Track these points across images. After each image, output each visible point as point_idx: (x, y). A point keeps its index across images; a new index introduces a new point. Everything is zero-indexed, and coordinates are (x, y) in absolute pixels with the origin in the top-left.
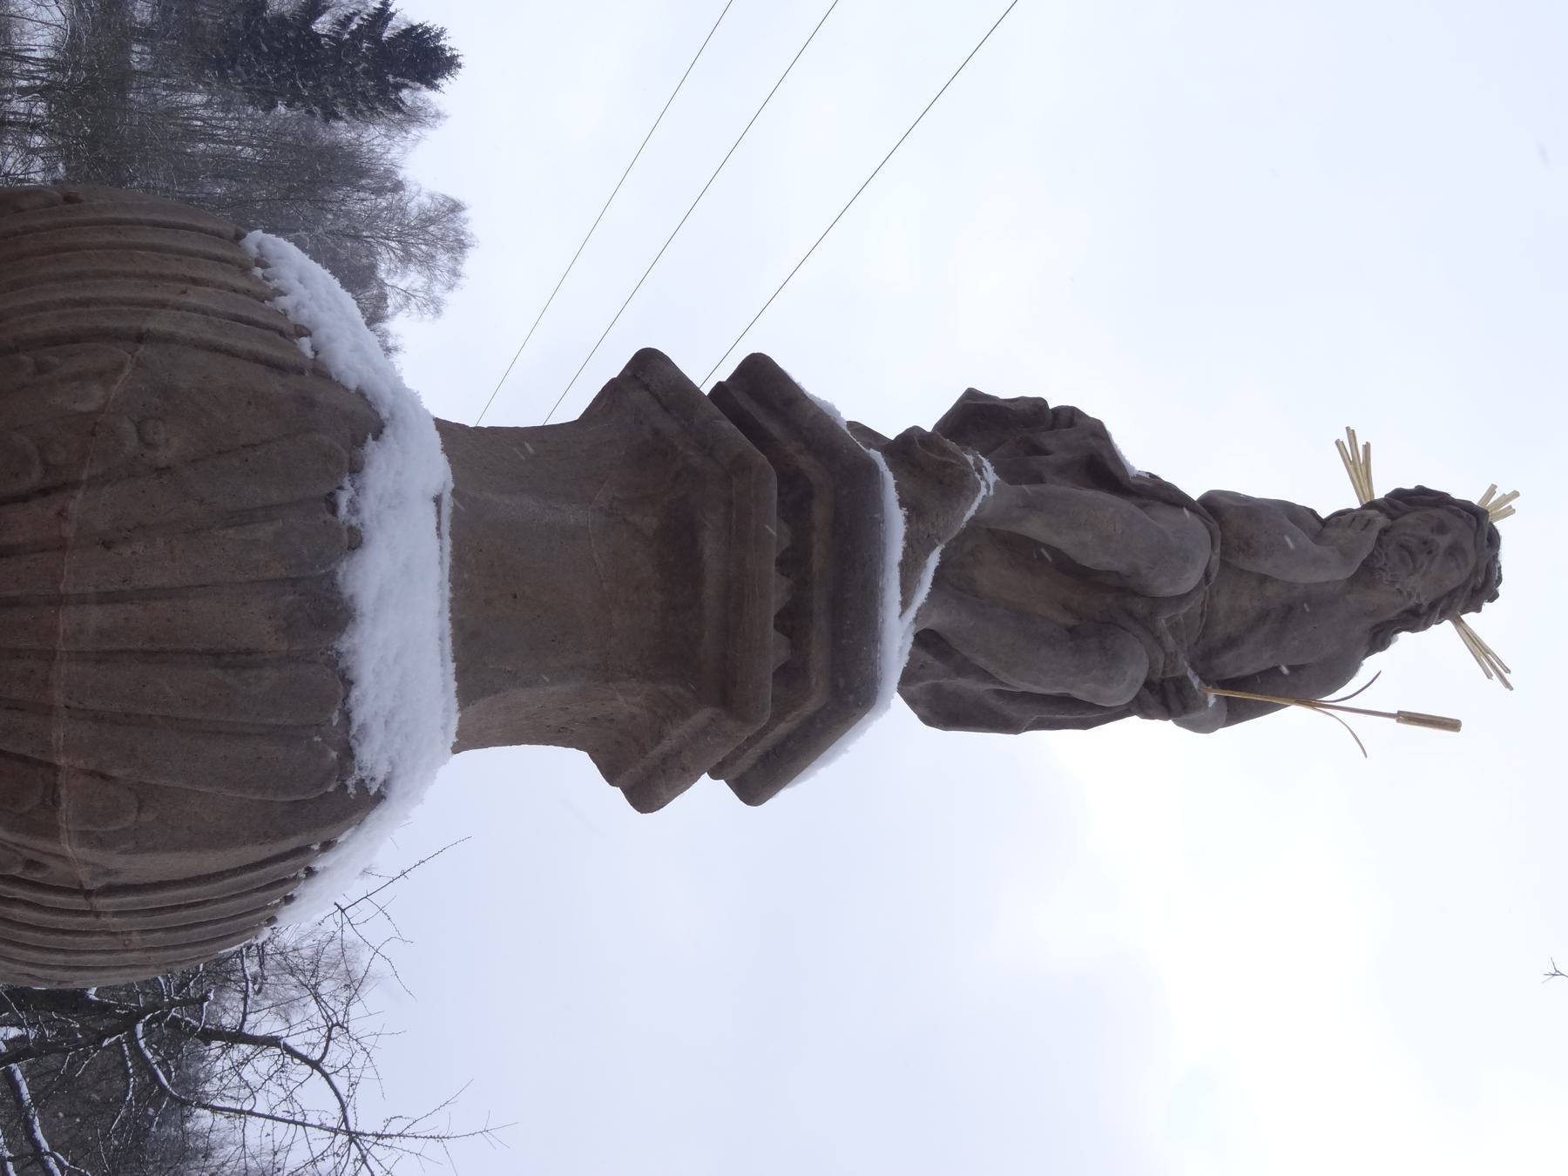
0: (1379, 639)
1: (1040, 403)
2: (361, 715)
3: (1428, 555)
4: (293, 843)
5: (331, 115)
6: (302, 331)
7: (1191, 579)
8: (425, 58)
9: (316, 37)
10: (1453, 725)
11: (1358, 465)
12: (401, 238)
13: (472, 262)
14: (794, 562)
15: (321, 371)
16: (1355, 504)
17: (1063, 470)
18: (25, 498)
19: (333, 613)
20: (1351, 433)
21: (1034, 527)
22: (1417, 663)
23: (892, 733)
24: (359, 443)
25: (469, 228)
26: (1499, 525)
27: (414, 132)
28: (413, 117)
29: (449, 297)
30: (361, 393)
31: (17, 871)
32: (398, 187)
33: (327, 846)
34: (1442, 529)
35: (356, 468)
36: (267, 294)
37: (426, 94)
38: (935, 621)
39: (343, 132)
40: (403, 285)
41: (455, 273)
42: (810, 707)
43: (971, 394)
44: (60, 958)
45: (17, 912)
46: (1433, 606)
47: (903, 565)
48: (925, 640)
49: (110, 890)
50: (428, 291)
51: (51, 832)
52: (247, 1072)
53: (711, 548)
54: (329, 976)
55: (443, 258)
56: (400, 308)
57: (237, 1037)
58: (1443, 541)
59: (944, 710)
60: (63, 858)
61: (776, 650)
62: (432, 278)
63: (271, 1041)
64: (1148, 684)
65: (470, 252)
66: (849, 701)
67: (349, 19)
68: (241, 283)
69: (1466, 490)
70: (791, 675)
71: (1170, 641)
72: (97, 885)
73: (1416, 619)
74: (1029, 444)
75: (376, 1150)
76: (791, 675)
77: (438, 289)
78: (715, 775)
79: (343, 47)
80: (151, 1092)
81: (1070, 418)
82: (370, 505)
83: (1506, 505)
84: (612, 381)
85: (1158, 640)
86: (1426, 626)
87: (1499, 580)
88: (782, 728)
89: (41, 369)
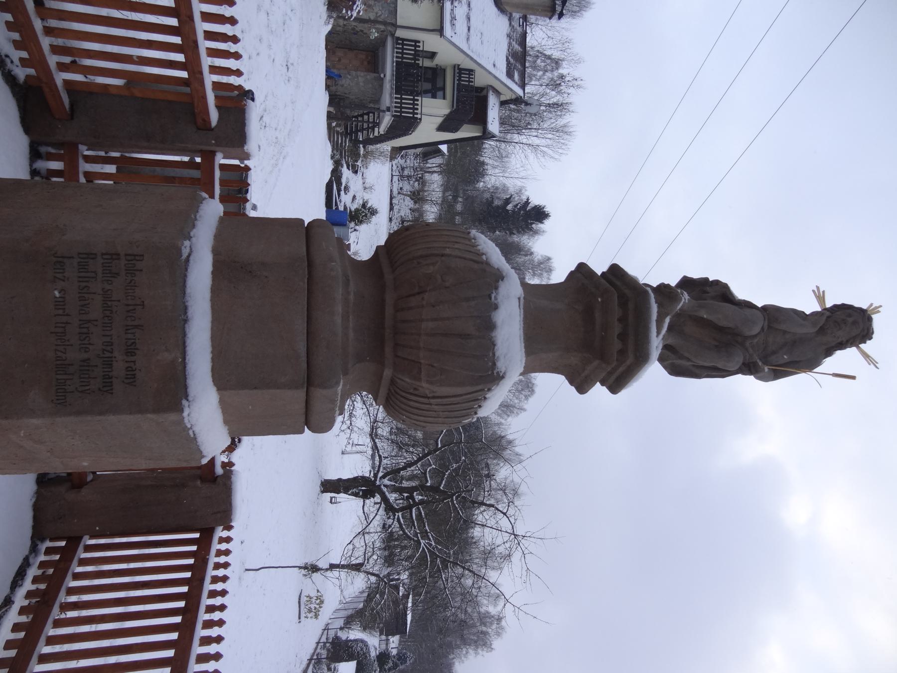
0: (829, 353)
1: (707, 279)
2: (497, 354)
3: (846, 326)
4: (480, 387)
5: (512, 233)
6: (483, 254)
7: (756, 330)
8: (540, 214)
9: (508, 211)
10: (853, 378)
11: (821, 298)
12: (532, 269)
14: (623, 320)
15: (488, 263)
16: (819, 309)
17: (713, 298)
18: (414, 295)
19: (489, 326)
20: (818, 288)
22: (844, 359)
23: (654, 372)
24: (498, 281)
25: (553, 265)
26: (873, 316)
27: (536, 237)
28: (536, 232)
30: (498, 269)
31: (411, 391)
32: (532, 254)
33: (489, 390)
34: (850, 316)
35: (496, 288)
36: (475, 246)
37: (540, 225)
38: (670, 341)
39: (515, 238)
42: (628, 362)
43: (685, 277)
44: (422, 418)
45: (412, 403)
46: (847, 341)
47: (657, 321)
48: (666, 347)
49: (434, 397)
51: (420, 380)
52: (485, 513)
53: (598, 315)
54: (511, 492)
55: (545, 274)
57: (482, 504)
58: (850, 320)
59: (676, 370)
60: (422, 387)
61: (617, 345)
63: (492, 506)
64: (743, 364)
66: (640, 360)
68: (468, 243)
69: (861, 303)
70: (622, 352)
71: (751, 350)
72: (431, 395)
73: (842, 346)
74: (708, 292)
75: (523, 541)
76: (622, 352)
78: (602, 385)
80: (458, 518)
81: (717, 283)
82: (500, 298)
83: (876, 310)
84: (572, 273)
85: (747, 349)
86: (845, 348)
87: (873, 333)
88: (621, 369)
89: (419, 263)
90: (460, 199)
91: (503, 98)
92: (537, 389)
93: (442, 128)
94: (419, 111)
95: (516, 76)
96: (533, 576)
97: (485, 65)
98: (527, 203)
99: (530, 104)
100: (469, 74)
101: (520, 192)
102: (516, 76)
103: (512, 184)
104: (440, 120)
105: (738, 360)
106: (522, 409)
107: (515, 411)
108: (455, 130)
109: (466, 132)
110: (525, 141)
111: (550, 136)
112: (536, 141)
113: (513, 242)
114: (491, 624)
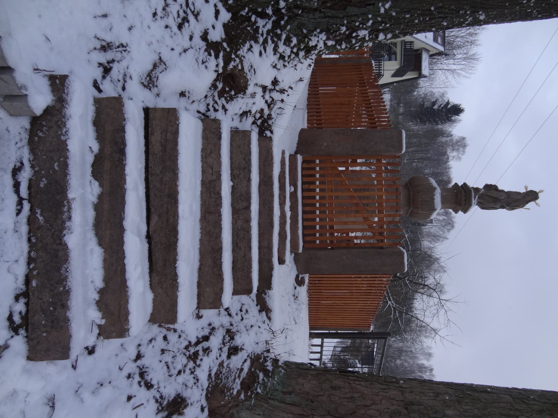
3: (531, 196)
5: (437, 124)
8: (457, 110)
9: (434, 110)
11: (526, 188)
12: (452, 146)
13: (468, 149)
19: (433, 199)
21: (488, 194)
22: (531, 205)
28: (454, 121)
29: (462, 156)
32: (451, 136)
39: (440, 127)
40: (452, 155)
41: (464, 152)
50: (458, 156)
55: (461, 149)
56: (452, 160)
62: (459, 153)
65: (467, 147)
67: (441, 105)
70: (465, 204)
73: (530, 201)
76: (465, 204)
77: (460, 155)
79: (440, 110)
90: (402, 105)
91: (431, 53)
92: (456, 225)
93: (394, 76)
94: (382, 69)
95: (439, 40)
96: (451, 323)
97: (420, 38)
98: (448, 103)
99: (448, 55)
100: (411, 44)
101: (443, 95)
102: (439, 40)
103: (437, 91)
104: (393, 72)
105: (499, 205)
106: (446, 238)
107: (441, 239)
108: (402, 76)
109: (409, 76)
110: (445, 68)
111: (463, 63)
112: (454, 67)
113: (438, 129)
114: (426, 372)
